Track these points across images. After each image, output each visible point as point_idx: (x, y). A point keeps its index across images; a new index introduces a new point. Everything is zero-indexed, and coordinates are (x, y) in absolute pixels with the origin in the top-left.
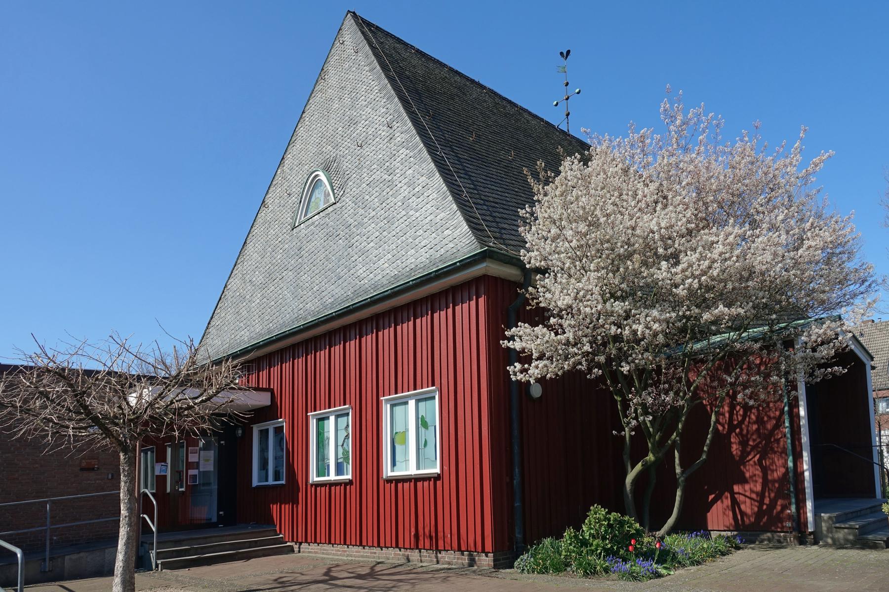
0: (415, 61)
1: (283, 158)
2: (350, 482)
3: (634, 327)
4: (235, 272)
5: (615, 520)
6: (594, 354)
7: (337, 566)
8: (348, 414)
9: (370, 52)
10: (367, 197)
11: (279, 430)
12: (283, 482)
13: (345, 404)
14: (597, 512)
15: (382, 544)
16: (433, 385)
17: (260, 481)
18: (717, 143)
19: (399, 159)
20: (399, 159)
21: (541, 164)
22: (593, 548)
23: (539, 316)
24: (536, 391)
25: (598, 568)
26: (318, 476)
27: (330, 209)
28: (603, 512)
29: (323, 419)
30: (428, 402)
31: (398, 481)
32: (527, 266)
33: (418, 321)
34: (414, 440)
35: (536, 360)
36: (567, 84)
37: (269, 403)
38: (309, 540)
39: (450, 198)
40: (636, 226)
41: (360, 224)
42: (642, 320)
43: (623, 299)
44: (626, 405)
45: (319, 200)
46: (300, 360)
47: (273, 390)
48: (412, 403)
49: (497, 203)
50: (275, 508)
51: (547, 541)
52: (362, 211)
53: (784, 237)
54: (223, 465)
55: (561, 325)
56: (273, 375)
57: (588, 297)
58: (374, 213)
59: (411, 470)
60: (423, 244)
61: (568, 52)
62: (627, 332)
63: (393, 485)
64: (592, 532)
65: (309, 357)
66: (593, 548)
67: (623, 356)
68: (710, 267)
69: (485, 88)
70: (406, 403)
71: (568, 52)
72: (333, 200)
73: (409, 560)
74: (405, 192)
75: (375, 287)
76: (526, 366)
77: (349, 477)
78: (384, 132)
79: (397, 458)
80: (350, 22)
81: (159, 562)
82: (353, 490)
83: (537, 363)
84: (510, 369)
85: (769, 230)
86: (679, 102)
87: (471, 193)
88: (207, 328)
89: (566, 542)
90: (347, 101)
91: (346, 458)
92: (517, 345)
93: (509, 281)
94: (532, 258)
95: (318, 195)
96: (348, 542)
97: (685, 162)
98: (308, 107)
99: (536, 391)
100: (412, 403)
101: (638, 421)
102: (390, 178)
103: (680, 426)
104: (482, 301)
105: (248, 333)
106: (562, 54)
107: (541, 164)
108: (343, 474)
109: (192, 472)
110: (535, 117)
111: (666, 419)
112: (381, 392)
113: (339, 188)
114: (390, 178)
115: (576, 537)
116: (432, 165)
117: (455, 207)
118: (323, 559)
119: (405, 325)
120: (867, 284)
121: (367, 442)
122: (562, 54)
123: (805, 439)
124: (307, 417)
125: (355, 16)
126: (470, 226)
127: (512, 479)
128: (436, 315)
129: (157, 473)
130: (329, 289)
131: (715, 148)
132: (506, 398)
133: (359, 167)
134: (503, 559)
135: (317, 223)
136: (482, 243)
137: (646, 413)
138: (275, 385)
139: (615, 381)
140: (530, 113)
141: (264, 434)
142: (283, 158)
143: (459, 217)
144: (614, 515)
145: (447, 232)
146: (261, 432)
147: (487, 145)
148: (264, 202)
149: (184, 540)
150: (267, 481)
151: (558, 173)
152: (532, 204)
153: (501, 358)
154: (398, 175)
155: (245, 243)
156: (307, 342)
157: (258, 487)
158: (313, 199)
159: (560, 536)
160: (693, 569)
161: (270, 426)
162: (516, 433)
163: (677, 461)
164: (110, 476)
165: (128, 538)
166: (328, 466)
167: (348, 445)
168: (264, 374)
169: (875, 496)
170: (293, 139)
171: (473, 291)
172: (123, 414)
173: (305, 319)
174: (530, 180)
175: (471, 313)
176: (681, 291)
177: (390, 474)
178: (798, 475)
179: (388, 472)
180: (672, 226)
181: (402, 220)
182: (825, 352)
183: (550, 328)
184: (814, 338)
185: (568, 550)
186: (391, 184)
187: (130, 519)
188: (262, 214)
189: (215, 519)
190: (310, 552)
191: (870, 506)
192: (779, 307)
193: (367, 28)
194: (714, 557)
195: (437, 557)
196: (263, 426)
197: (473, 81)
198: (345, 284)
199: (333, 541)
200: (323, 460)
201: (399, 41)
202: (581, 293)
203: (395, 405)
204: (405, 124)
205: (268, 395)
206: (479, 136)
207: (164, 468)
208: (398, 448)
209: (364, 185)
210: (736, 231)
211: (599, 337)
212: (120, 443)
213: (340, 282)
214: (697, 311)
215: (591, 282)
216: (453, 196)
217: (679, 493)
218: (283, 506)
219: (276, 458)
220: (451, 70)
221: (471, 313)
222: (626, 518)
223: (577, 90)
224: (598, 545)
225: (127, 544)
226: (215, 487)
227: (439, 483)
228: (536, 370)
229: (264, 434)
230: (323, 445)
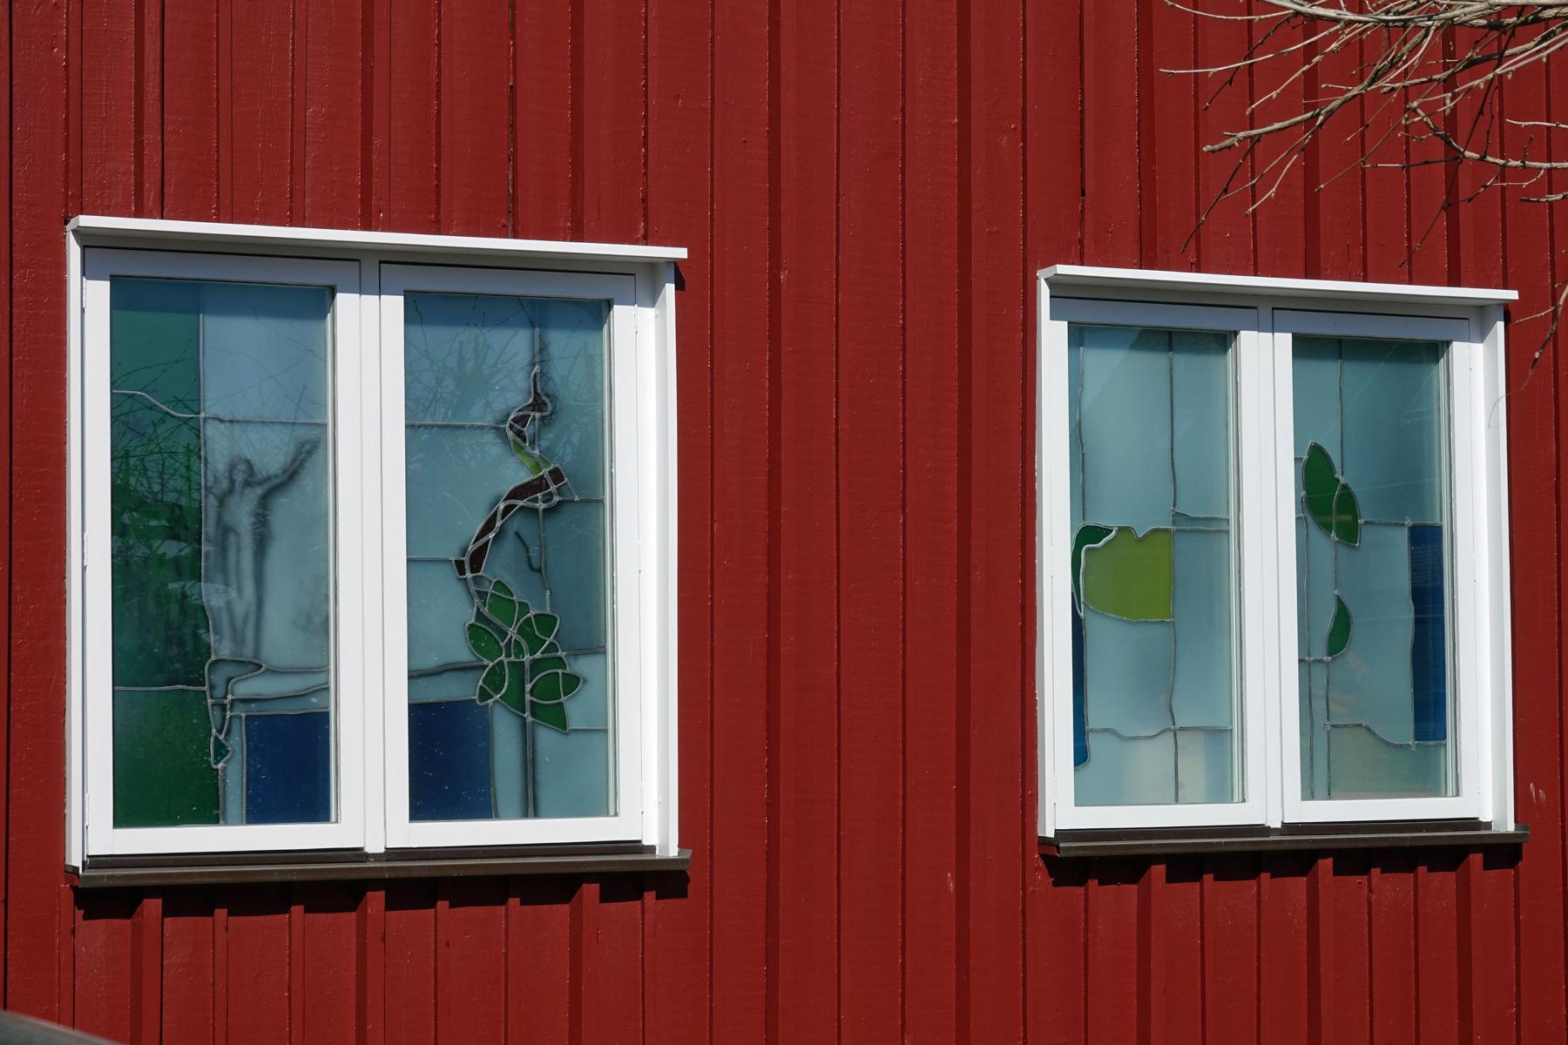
26: (124, 817)
108: (483, 809)
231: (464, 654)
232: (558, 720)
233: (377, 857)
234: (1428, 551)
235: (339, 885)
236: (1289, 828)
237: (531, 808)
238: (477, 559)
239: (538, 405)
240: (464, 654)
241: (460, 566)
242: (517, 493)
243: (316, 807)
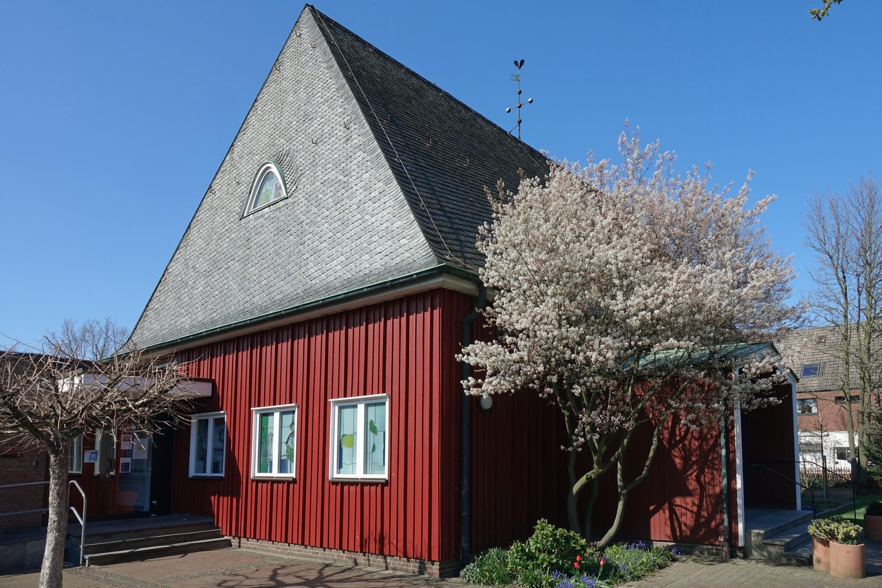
0: (373, 60)
1: (232, 145)
2: (294, 481)
3: (588, 353)
4: (177, 256)
5: (561, 536)
6: (546, 374)
7: (283, 567)
8: (293, 412)
9: (328, 49)
10: (321, 196)
11: (219, 422)
12: (223, 475)
13: (291, 402)
14: (544, 529)
15: (325, 545)
16: (384, 392)
18: (669, 176)
19: (355, 162)
20: (355, 162)
21: (501, 183)
22: (539, 562)
23: (494, 334)
24: (487, 403)
25: (544, 582)
26: (260, 471)
27: (282, 203)
28: (550, 528)
29: (267, 415)
30: (378, 408)
31: (344, 483)
32: (485, 285)
33: (371, 326)
34: (361, 444)
35: (491, 376)
36: (520, 93)
38: (248, 536)
39: (408, 207)
40: (593, 254)
41: (312, 223)
42: (596, 346)
43: (576, 323)
44: (574, 421)
45: (270, 192)
46: (245, 353)
47: (214, 380)
48: (361, 407)
49: (453, 213)
50: (212, 498)
51: (493, 552)
52: (315, 210)
53: (730, 274)
54: (164, 462)
55: (516, 344)
56: (217, 365)
57: (545, 320)
58: (327, 213)
59: (359, 474)
60: (378, 250)
61: (522, 62)
62: (581, 358)
63: (339, 487)
64: (538, 546)
65: (254, 351)
66: (539, 562)
67: (575, 377)
68: (663, 302)
69: (441, 91)
70: (355, 406)
71: (522, 62)
72: (284, 194)
73: (356, 564)
74: (361, 195)
75: (327, 288)
76: (480, 381)
77: (292, 475)
78: (340, 132)
79: (344, 461)
80: (307, 15)
81: (87, 557)
82: (297, 488)
83: (490, 379)
84: (464, 383)
85: (716, 267)
86: (636, 136)
87: (428, 202)
88: (145, 310)
89: (512, 552)
90: (303, 95)
91: (290, 456)
92: (472, 360)
93: (464, 294)
94: (490, 276)
95: (269, 187)
96: (289, 540)
97: (640, 194)
98: (260, 97)
99: (487, 403)
100: (361, 407)
101: (585, 439)
102: (346, 179)
103: (625, 441)
104: (436, 312)
105: (189, 321)
106: (516, 62)
107: (501, 183)
108: (286, 472)
109: (123, 460)
110: (489, 123)
111: (612, 438)
112: (329, 394)
113: (291, 180)
114: (346, 179)
115: (523, 550)
116: (390, 172)
117: (412, 217)
118: (263, 556)
119: (357, 329)
120: (801, 320)
121: (313, 442)
122: (516, 62)
123: (739, 461)
124: (250, 412)
125: (313, 10)
126: (427, 238)
127: (460, 489)
128: (389, 322)
129: (86, 461)
130: (278, 285)
131: (667, 180)
132: (457, 410)
133: (313, 165)
134: (449, 567)
135: (267, 216)
136: (439, 255)
137: (593, 430)
138: (217, 376)
139: (565, 398)
140: (484, 119)
141: (203, 424)
142: (232, 145)
143: (416, 228)
144: (560, 531)
145: (403, 241)
146: (200, 421)
147: (449, 157)
148: (210, 187)
149: (113, 533)
150: (204, 471)
151: (516, 192)
152: (490, 223)
153: (455, 372)
154: (354, 178)
155: (189, 227)
156: (252, 336)
157: (195, 478)
158: (263, 191)
159: (506, 547)
160: (635, 583)
161: (211, 417)
162: (466, 443)
163: (619, 476)
164: (34, 464)
165: (56, 544)
166: (271, 462)
167: (292, 443)
168: (205, 364)
169: (795, 508)
170: (244, 127)
171: (429, 302)
172: (56, 415)
173: (252, 313)
174: (490, 198)
175: (425, 324)
176: (634, 322)
177: (336, 476)
178: (731, 492)
179: (334, 474)
180: (628, 260)
181: (356, 224)
182: (764, 384)
183: (503, 344)
184: (753, 370)
185: (514, 563)
186: (346, 186)
187: (59, 523)
188: (208, 200)
189: (147, 509)
190: (248, 548)
191: (793, 520)
192: (724, 339)
193: (330, 28)
194: (652, 571)
196: (203, 416)
197: (429, 84)
198: (295, 281)
199: (273, 539)
200: (266, 455)
201: (357, 38)
202: (538, 317)
203: (344, 407)
204: (363, 127)
205: (210, 385)
206: (435, 142)
207: (94, 456)
208: (345, 450)
209: (318, 183)
210: (689, 270)
211: (553, 359)
212: (51, 444)
213: (290, 278)
214: (648, 341)
215: (547, 309)
216: (410, 206)
217: (620, 505)
218: (221, 498)
219: (217, 450)
220: (408, 71)
221: (425, 324)
222: (572, 533)
223: (530, 100)
224: (544, 560)
225: (54, 550)
226: (148, 474)
227: (386, 489)
228: (489, 386)
229: (203, 424)
230: (266, 441)
235: (273, 482)
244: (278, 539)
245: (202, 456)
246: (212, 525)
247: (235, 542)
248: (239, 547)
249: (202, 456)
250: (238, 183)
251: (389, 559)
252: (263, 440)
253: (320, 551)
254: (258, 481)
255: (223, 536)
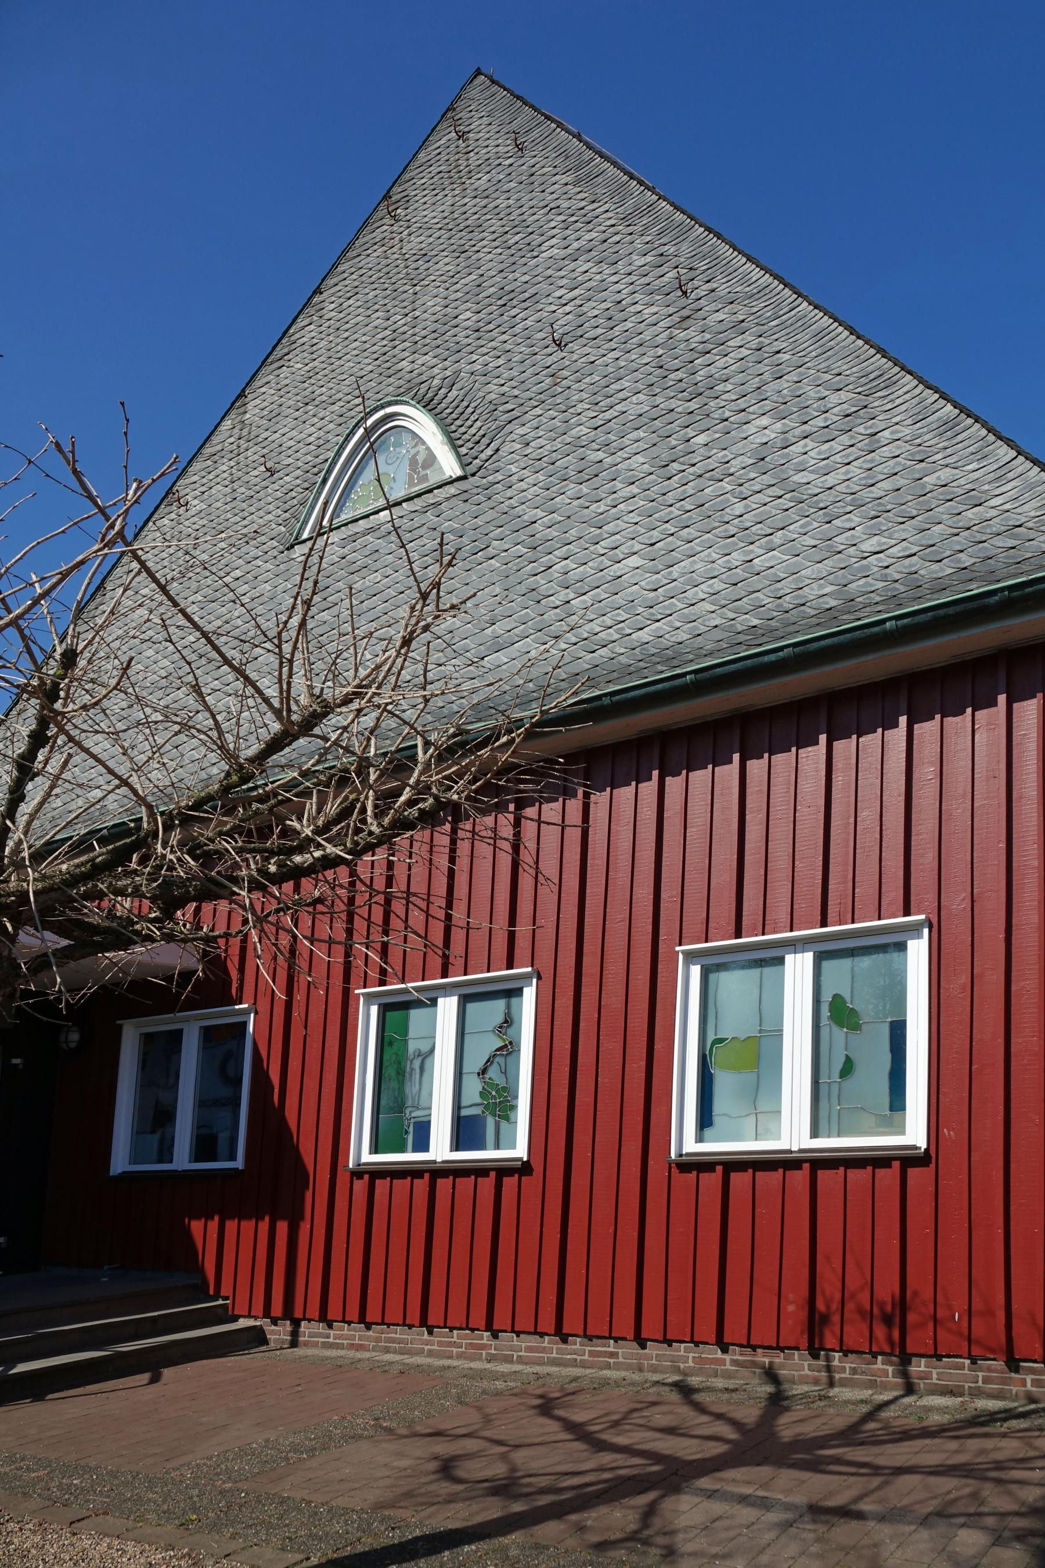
1: (242, 395)
2: (524, 1169)
12: (239, 1163)
17: (134, 1159)
26: (375, 1149)
29: (406, 1006)
37: (835, 743)
50: (196, 1227)
59: (792, 1132)
108: (481, 1146)
146: (148, 1039)
157: (125, 1176)
170: (279, 352)
177: (691, 1146)
195: (905, 1374)
203: (720, 967)
218: (231, 1226)
231: (479, 1100)
232: (507, 1119)
233: (795, 1152)
234: (898, 1032)
235: (437, 1172)
236: (444, 1162)
237: (497, 1147)
238: (484, 1071)
239: (506, 1022)
240: (479, 1100)
241: (479, 1074)
242: (498, 1050)
243: (426, 1149)
244: (457, 1316)
245: (157, 1118)
246: (200, 1291)
247: (278, 1333)
248: (294, 1344)
249: (157, 1118)
250: (271, 472)
251: (919, 1366)
252: (390, 1071)
253: (627, 1351)
254: (376, 1173)
255: (235, 1319)
